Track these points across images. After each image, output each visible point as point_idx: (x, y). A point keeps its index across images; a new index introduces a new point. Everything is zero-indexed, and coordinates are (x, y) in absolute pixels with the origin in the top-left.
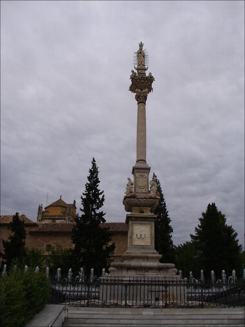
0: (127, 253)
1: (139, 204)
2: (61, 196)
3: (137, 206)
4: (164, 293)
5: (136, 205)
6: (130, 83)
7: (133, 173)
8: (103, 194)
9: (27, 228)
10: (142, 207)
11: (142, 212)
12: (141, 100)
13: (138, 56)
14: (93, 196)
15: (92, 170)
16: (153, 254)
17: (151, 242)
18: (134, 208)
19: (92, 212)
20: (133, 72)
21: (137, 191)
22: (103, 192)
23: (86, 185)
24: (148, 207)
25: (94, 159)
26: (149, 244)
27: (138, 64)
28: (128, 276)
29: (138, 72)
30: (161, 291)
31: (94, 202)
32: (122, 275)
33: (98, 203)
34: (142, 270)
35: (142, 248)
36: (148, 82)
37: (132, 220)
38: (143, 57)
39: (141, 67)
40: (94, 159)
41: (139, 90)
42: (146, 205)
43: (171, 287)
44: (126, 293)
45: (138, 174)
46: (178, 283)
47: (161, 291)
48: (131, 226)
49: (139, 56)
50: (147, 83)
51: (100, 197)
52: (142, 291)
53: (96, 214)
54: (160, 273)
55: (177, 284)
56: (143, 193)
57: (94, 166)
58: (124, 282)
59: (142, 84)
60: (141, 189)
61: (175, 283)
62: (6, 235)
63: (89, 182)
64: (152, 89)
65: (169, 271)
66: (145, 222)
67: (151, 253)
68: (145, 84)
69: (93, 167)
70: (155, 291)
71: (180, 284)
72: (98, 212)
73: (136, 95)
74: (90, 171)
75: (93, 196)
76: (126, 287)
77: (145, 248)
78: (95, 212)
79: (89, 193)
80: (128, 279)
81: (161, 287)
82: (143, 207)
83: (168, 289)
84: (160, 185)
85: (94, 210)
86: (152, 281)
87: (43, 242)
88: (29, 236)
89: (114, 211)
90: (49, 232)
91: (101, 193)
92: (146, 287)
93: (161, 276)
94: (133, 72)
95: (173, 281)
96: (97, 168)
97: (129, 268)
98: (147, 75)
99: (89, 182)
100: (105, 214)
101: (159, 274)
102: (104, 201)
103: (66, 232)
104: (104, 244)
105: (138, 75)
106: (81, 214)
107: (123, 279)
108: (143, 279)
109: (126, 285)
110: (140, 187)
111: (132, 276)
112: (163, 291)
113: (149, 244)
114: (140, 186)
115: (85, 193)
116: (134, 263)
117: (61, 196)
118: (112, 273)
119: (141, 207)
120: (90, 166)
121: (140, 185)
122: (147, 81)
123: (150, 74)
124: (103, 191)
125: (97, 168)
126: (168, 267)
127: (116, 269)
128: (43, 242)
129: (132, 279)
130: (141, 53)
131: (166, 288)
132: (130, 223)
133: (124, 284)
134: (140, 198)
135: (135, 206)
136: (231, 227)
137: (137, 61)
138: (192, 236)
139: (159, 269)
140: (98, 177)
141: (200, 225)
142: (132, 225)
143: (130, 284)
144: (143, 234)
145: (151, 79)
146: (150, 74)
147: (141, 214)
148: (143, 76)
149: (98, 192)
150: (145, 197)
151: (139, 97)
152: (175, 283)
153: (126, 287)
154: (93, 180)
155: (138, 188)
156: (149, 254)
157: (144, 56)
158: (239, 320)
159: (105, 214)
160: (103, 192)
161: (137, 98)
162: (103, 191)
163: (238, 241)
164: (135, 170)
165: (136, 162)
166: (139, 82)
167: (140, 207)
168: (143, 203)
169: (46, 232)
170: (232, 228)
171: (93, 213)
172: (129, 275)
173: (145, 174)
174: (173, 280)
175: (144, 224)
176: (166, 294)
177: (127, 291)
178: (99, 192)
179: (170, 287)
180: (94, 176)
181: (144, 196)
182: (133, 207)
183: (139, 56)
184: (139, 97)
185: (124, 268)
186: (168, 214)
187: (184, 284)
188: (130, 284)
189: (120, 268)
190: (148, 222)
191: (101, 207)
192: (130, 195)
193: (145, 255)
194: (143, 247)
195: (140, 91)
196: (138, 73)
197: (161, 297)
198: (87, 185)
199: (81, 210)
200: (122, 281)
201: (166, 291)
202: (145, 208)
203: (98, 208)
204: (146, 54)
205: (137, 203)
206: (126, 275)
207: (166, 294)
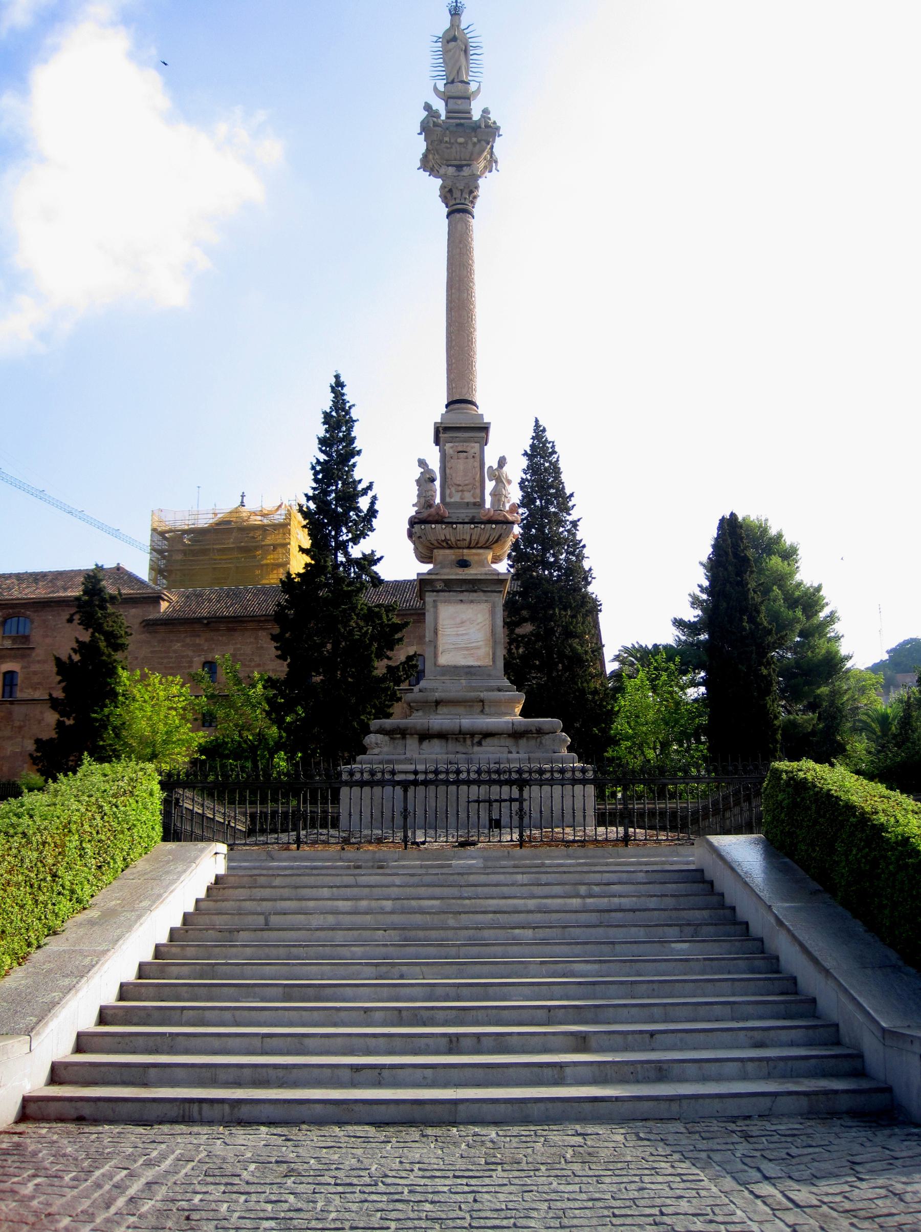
0: (421, 691)
1: (453, 539)
2: (243, 496)
3: (450, 547)
4: (515, 806)
5: (444, 544)
6: (420, 145)
7: (437, 442)
8: (370, 494)
9: (134, 610)
10: (465, 551)
11: (464, 564)
12: (458, 201)
13: (445, 52)
14: (336, 503)
15: (334, 414)
16: (499, 690)
17: (494, 654)
18: (439, 553)
19: (339, 554)
20: (428, 107)
21: (448, 500)
22: (370, 487)
23: (313, 468)
24: (481, 548)
25: (337, 377)
26: (487, 662)
27: (447, 79)
28: (434, 755)
29: (446, 105)
30: (505, 801)
31: (339, 521)
32: (403, 757)
33: (356, 523)
34: (465, 739)
35: (467, 673)
36: (479, 141)
37: (433, 591)
38: (462, 54)
39: (457, 90)
40: (337, 377)
41: (451, 170)
42: (477, 543)
43: (535, 788)
44: (406, 809)
45: (451, 445)
46: (556, 775)
47: (505, 801)
48: (432, 610)
49: (450, 51)
50: (474, 144)
51: (363, 503)
52: (377, 800)
53: (351, 561)
54: (517, 746)
55: (552, 779)
56: (468, 504)
57: (338, 401)
58: (398, 778)
59: (458, 149)
60: (460, 494)
61: (548, 775)
62: (64, 638)
63: (322, 457)
64: (496, 162)
65: (543, 741)
66: (473, 596)
67: (491, 689)
68: (470, 146)
69: (335, 403)
70: (501, 801)
71: (541, 780)
72: (356, 552)
73: (442, 188)
74: (327, 417)
75: (336, 503)
76: (406, 791)
77: (475, 674)
78: (346, 554)
79: (326, 493)
80: (411, 767)
81: (506, 789)
82: (469, 548)
83: (526, 795)
84: (558, 460)
85: (343, 546)
86: (436, 772)
87: (190, 653)
88: (143, 636)
89: (393, 554)
90: (209, 618)
91: (365, 492)
92: (464, 788)
93: (515, 757)
94: (428, 107)
95: (541, 772)
96: (350, 407)
97: (425, 736)
98: (476, 115)
99: (322, 457)
100: (382, 557)
101: (514, 749)
102: (375, 517)
103: (262, 619)
104: (380, 656)
105: (447, 118)
106: (298, 563)
107: (398, 767)
108: (432, 768)
109: (405, 785)
110: (459, 485)
111: (434, 756)
112: (511, 800)
113: (487, 662)
114: (458, 483)
115: (311, 493)
116: (439, 721)
117: (243, 496)
118: (376, 751)
119: (461, 551)
120: (326, 402)
121: (459, 479)
122: (475, 140)
123: (486, 111)
124: (371, 484)
125: (350, 407)
126: (540, 729)
127: (387, 738)
128: (190, 653)
129: (421, 767)
130: (454, 39)
131: (521, 790)
132: (429, 598)
133: (399, 783)
134: (456, 523)
135: (444, 548)
136: (819, 589)
137: (444, 73)
138: (679, 623)
139: (516, 735)
140: (353, 434)
141: (706, 583)
142: (435, 607)
143: (415, 783)
144: (465, 635)
145: (485, 132)
146: (486, 111)
147: (460, 571)
148: (462, 121)
149: (355, 489)
150: (474, 517)
151: (450, 191)
152: (548, 775)
153: (406, 791)
154: (337, 451)
155: (453, 490)
156: (486, 690)
157: (466, 51)
158: (667, 874)
159: (382, 557)
160: (370, 487)
161: (447, 194)
162: (371, 484)
163: (838, 638)
164: (441, 433)
165: (447, 406)
166: (450, 143)
167: (457, 550)
168: (468, 538)
169: (199, 620)
170: (821, 593)
171: (341, 558)
172: (424, 756)
173: (473, 444)
174: (540, 768)
175: (472, 602)
176: (521, 809)
177: (414, 803)
178: (360, 487)
179: (533, 787)
180: (341, 434)
181: (471, 515)
182: (435, 551)
183: (450, 51)
184: (450, 191)
185: (411, 734)
186: (586, 552)
187: (574, 779)
188: (415, 783)
189: (398, 736)
190: (481, 594)
191: (363, 535)
192: (425, 514)
193: (473, 694)
194: (469, 671)
195: (456, 174)
196: (448, 112)
197: (505, 820)
198: (318, 468)
199: (302, 550)
200: (393, 773)
201: (521, 800)
202: (474, 551)
203: (355, 540)
204: (472, 42)
205: (448, 537)
206: (416, 756)
207: (521, 809)
